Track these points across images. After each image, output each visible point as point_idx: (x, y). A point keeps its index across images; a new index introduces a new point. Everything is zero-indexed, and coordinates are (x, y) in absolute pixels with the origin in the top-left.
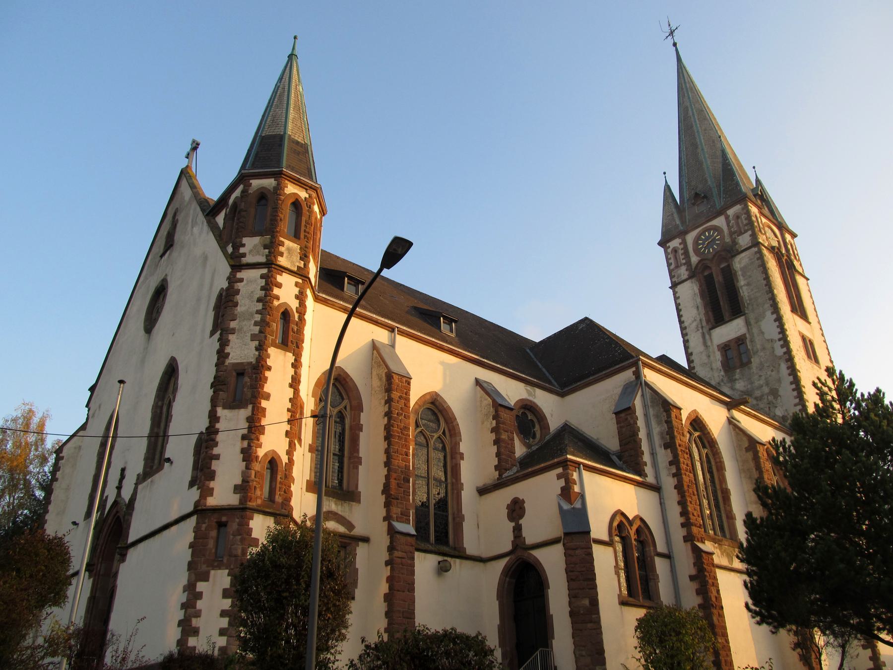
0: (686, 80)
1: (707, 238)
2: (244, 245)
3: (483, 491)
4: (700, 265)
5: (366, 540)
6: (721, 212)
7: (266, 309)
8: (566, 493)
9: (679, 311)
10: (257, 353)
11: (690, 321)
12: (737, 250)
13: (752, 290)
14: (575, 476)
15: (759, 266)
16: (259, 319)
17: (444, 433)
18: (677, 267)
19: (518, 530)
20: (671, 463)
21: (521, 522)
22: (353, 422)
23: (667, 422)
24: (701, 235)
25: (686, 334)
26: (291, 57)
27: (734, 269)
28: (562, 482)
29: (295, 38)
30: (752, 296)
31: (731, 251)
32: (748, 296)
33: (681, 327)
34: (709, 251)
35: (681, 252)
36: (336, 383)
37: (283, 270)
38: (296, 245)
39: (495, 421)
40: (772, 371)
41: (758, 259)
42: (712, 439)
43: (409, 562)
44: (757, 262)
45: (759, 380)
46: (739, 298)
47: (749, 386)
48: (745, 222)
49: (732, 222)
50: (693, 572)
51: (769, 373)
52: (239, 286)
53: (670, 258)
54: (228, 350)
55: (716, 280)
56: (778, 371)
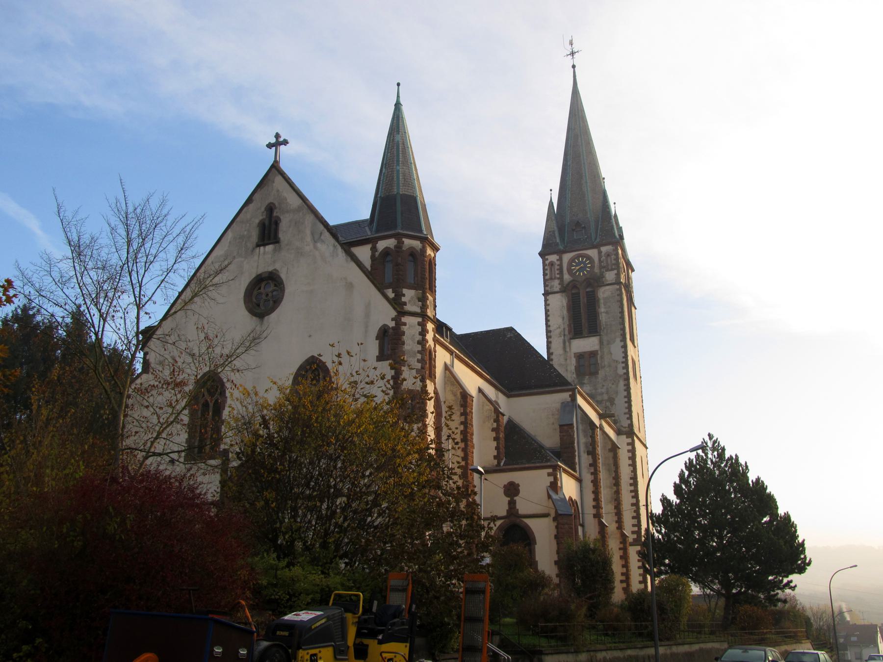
1: (580, 263)
2: (404, 295)
6: (596, 246)
9: (547, 316)
11: (555, 327)
12: (603, 283)
18: (551, 279)
19: (512, 504)
20: (591, 465)
21: (516, 498)
23: (591, 437)
26: (398, 106)
28: (551, 479)
29: (398, 85)
34: (579, 274)
35: (557, 267)
40: (613, 384)
41: (618, 295)
45: (602, 388)
47: (594, 391)
48: (614, 262)
51: (610, 385)
52: (404, 328)
53: (547, 270)
56: (617, 386)
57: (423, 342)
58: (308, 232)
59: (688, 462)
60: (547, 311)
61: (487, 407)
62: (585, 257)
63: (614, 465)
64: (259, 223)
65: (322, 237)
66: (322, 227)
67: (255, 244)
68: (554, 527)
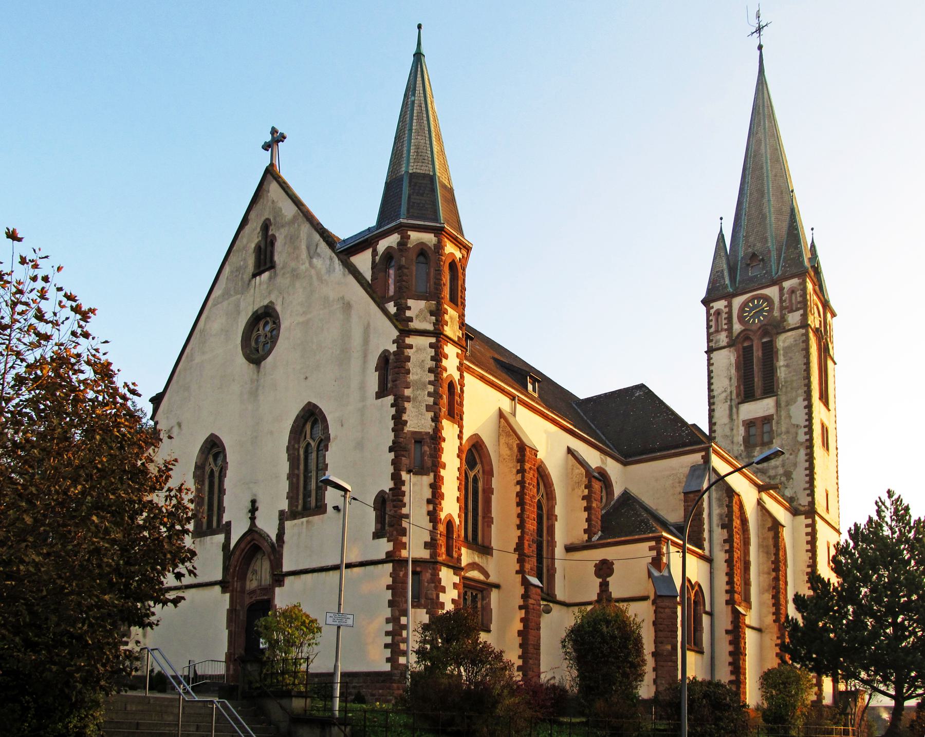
1: (755, 307)
2: (409, 308)
3: (569, 549)
4: (742, 335)
5: (497, 586)
7: (438, 381)
8: (657, 562)
9: (710, 378)
10: (433, 424)
11: (720, 391)
14: (664, 550)
15: (803, 350)
16: (432, 390)
18: (717, 331)
19: (604, 586)
20: (725, 541)
21: (608, 579)
23: (727, 506)
24: (749, 301)
25: (714, 404)
27: (776, 347)
28: (654, 553)
29: (419, 27)
30: (789, 379)
32: (785, 378)
33: (709, 395)
34: (754, 321)
35: (724, 316)
36: (473, 450)
38: (455, 313)
39: (587, 490)
40: (791, 454)
41: (803, 342)
42: (746, 518)
44: (801, 344)
46: (775, 378)
48: (799, 299)
49: (785, 296)
50: (730, 627)
53: (712, 320)
55: (755, 354)
56: (796, 456)
57: (437, 369)
58: (303, 247)
59: (853, 528)
60: (710, 372)
61: (577, 471)
63: (774, 547)
64: (255, 247)
66: (317, 237)
67: (251, 274)
68: (653, 612)
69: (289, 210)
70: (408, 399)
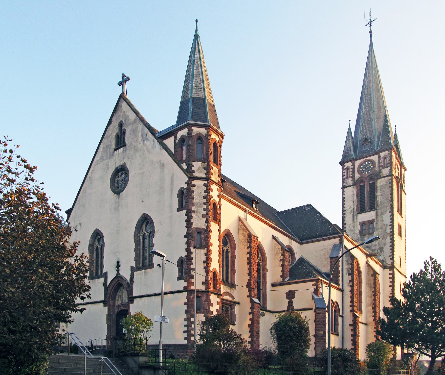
0: (373, 61)
1: (366, 166)
2: (193, 166)
3: (273, 285)
5: (238, 303)
6: (377, 153)
9: (343, 201)
10: (206, 224)
11: (348, 208)
13: (383, 198)
14: (320, 286)
15: (389, 187)
17: (229, 247)
18: (347, 178)
19: (290, 303)
20: (350, 281)
22: (233, 254)
23: (351, 264)
24: (363, 163)
26: (196, 36)
28: (315, 287)
29: (197, 21)
30: (382, 202)
31: (377, 176)
35: (351, 170)
37: (213, 182)
40: (383, 239)
41: (390, 183)
43: (258, 313)
44: (389, 184)
48: (388, 162)
50: (352, 323)
52: (193, 188)
53: (344, 172)
54: (192, 221)
55: (366, 189)
59: (413, 275)
60: (343, 198)
61: (277, 247)
62: (369, 161)
63: (374, 284)
65: (147, 137)
66: (146, 130)
67: (114, 149)
69: (132, 116)
70: (193, 212)
